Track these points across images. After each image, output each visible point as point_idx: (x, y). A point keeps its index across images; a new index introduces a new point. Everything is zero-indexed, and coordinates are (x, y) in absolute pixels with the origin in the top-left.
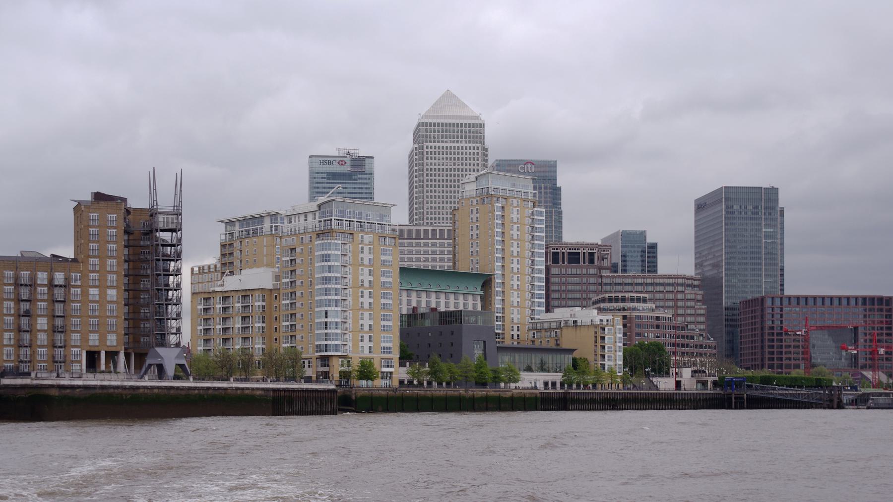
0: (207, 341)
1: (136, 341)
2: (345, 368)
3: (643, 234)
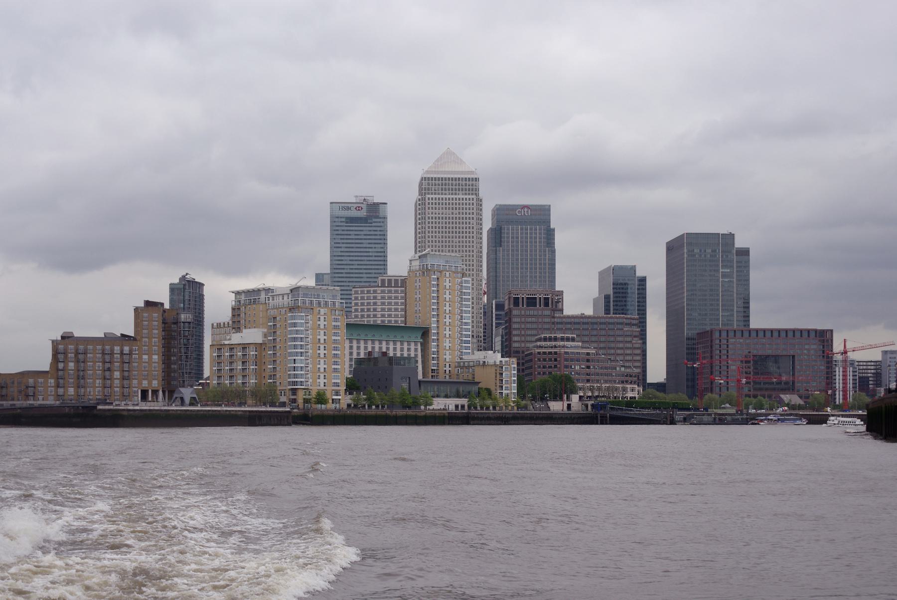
0: (219, 377)
1: (169, 383)
2: (307, 397)
3: (633, 269)
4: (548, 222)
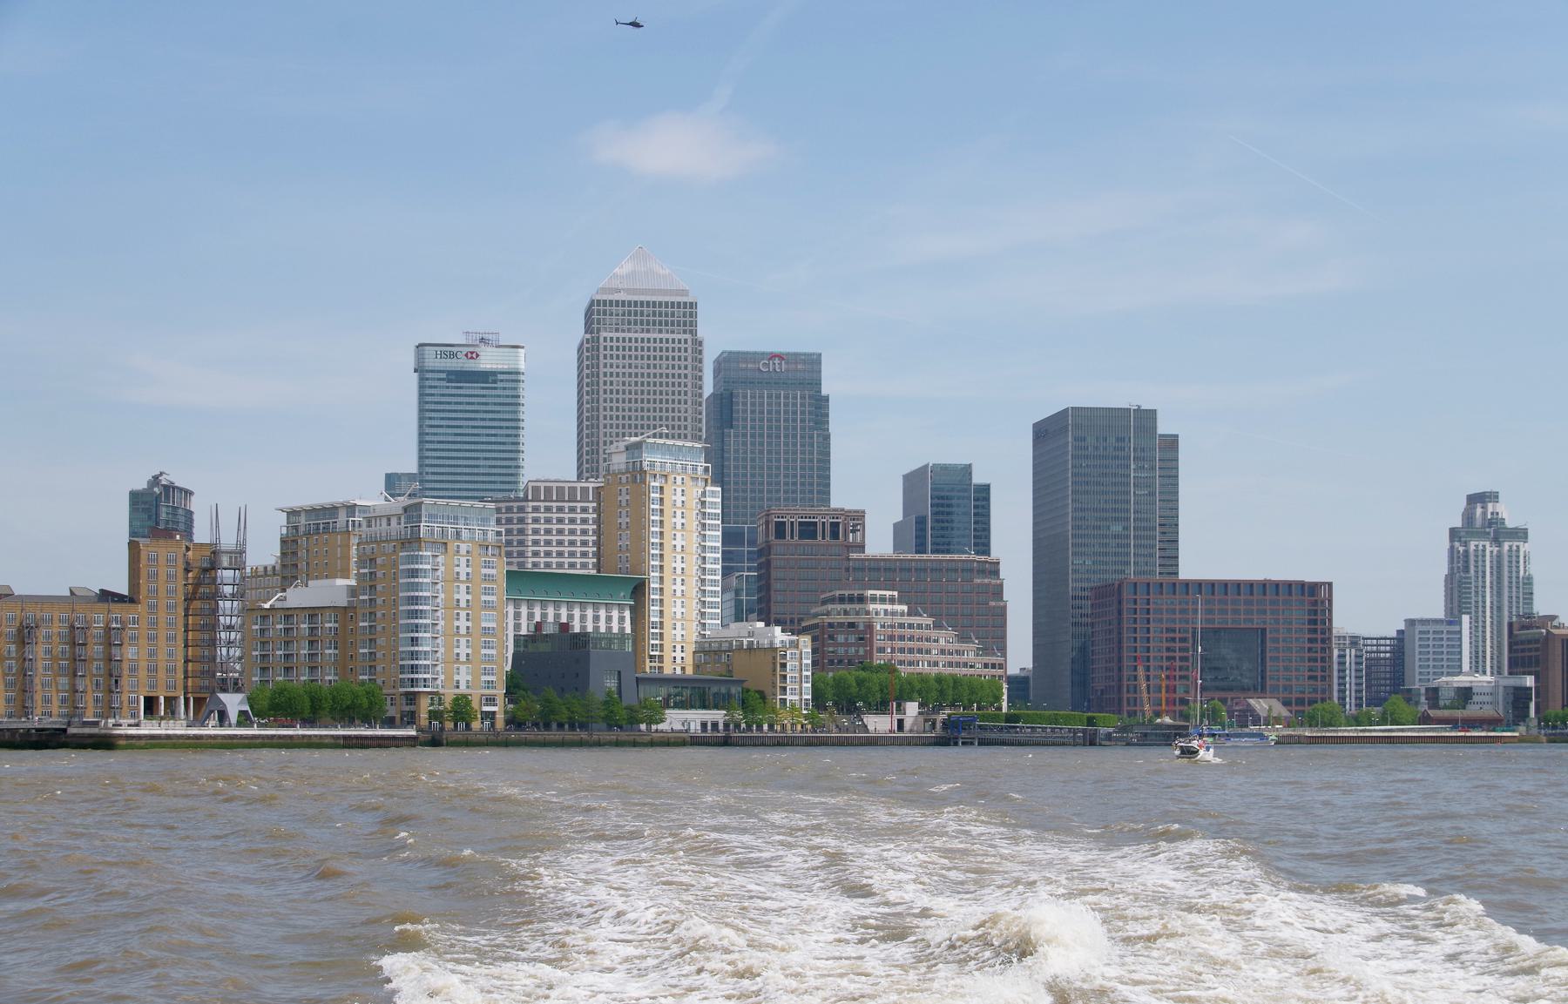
3: (967, 470)
4: (818, 384)
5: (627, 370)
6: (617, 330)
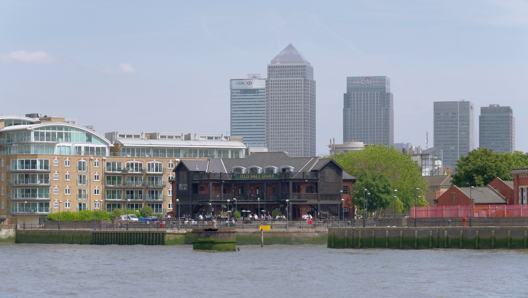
5: (279, 92)
6: (277, 77)
